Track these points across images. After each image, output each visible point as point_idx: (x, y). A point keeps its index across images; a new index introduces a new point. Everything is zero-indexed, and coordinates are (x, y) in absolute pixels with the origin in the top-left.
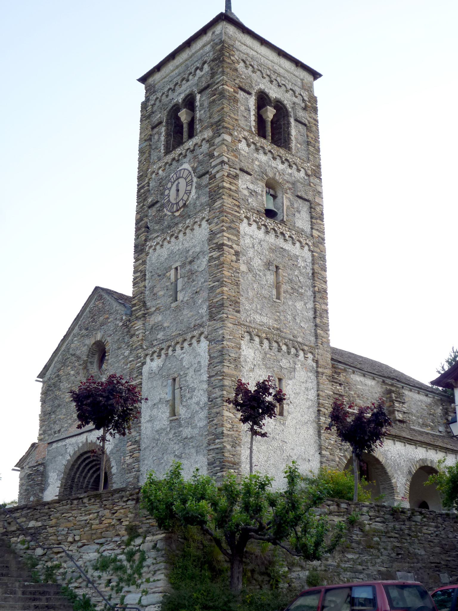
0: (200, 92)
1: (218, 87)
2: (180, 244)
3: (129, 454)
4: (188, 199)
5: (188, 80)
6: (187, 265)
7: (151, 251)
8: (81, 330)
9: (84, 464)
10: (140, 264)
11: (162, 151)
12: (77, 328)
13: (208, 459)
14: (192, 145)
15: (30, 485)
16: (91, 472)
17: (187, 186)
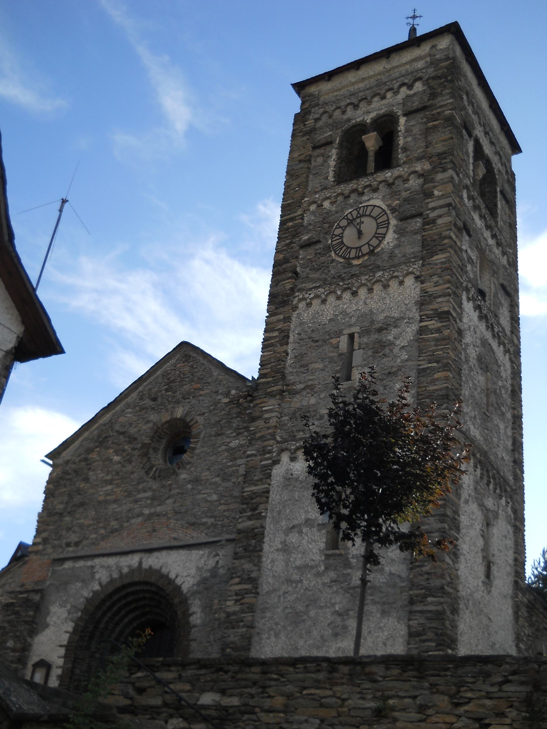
0: (405, 115)
1: (444, 112)
2: (361, 303)
3: (235, 598)
4: (378, 245)
7: (302, 305)
8: (141, 399)
9: (124, 602)
10: (279, 321)
11: (331, 178)
12: (134, 395)
13: (409, 627)
14: (391, 177)
15: (9, 622)
16: (131, 616)
17: (378, 228)
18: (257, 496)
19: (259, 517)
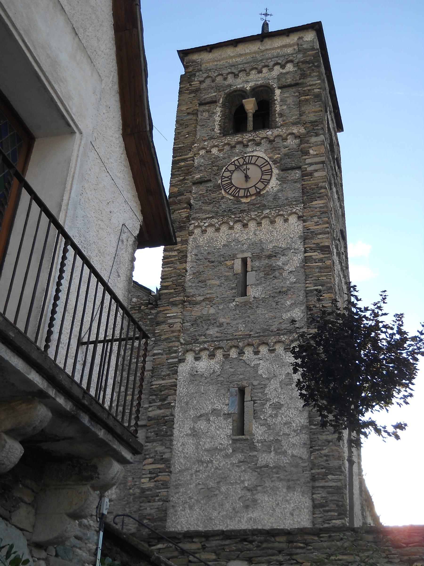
1: (313, 89)
5: (260, 72)
6: (263, 259)
7: (197, 231)
18: (166, 389)
19: (169, 406)
